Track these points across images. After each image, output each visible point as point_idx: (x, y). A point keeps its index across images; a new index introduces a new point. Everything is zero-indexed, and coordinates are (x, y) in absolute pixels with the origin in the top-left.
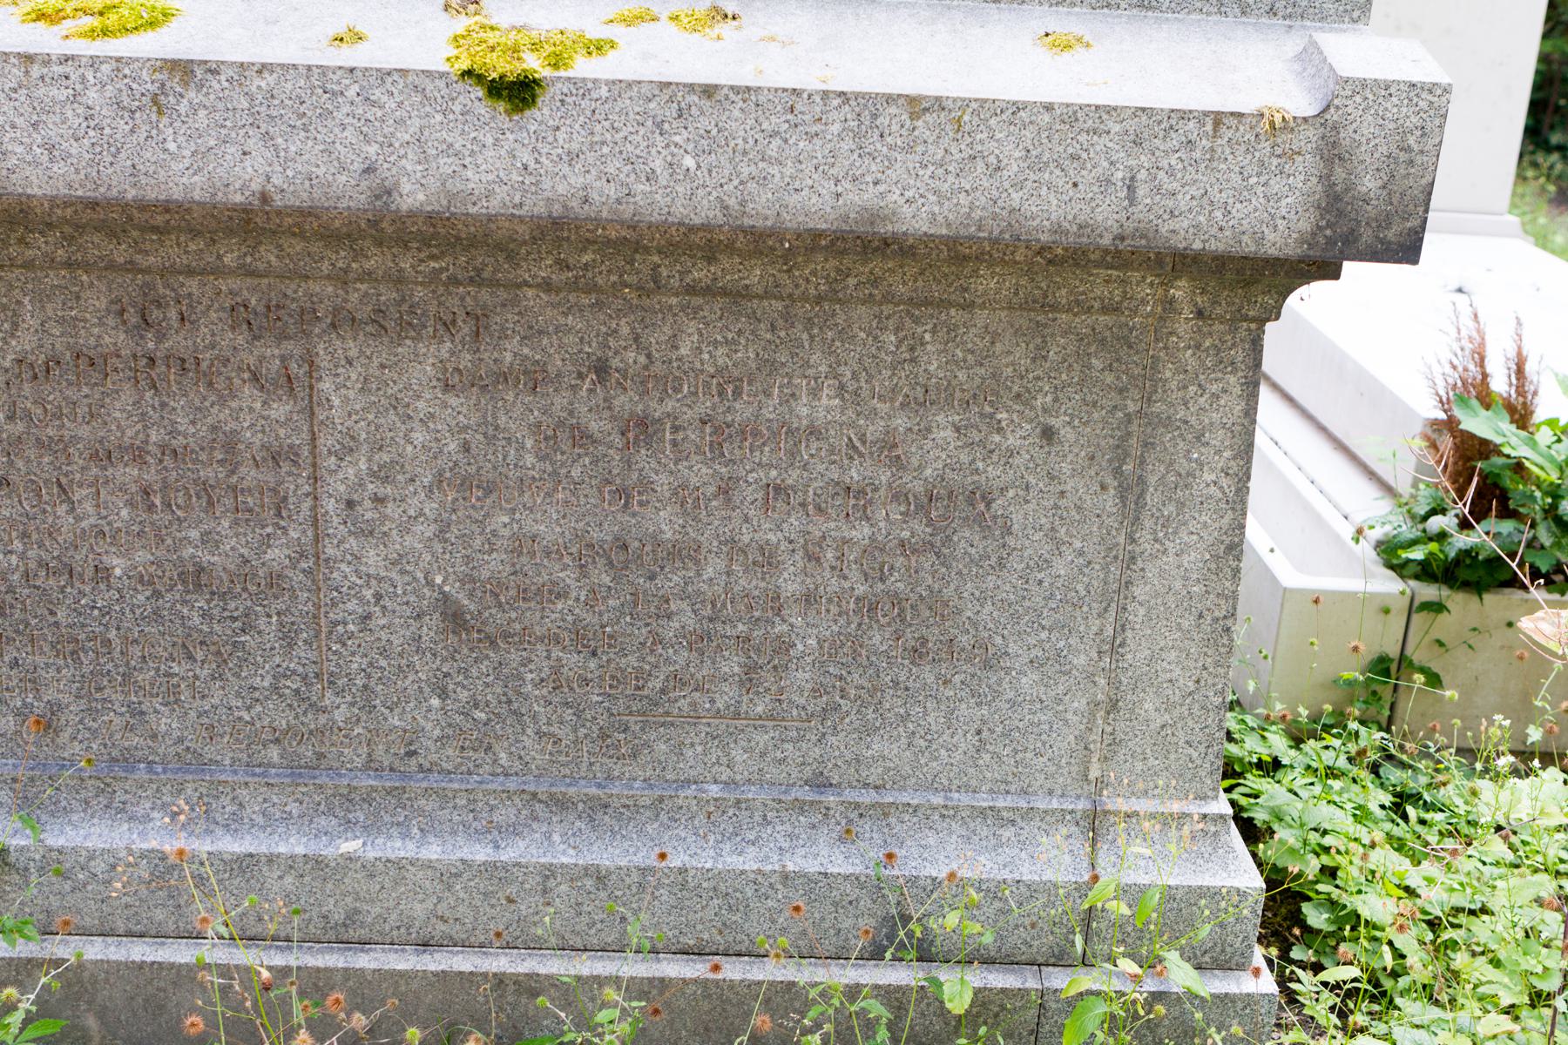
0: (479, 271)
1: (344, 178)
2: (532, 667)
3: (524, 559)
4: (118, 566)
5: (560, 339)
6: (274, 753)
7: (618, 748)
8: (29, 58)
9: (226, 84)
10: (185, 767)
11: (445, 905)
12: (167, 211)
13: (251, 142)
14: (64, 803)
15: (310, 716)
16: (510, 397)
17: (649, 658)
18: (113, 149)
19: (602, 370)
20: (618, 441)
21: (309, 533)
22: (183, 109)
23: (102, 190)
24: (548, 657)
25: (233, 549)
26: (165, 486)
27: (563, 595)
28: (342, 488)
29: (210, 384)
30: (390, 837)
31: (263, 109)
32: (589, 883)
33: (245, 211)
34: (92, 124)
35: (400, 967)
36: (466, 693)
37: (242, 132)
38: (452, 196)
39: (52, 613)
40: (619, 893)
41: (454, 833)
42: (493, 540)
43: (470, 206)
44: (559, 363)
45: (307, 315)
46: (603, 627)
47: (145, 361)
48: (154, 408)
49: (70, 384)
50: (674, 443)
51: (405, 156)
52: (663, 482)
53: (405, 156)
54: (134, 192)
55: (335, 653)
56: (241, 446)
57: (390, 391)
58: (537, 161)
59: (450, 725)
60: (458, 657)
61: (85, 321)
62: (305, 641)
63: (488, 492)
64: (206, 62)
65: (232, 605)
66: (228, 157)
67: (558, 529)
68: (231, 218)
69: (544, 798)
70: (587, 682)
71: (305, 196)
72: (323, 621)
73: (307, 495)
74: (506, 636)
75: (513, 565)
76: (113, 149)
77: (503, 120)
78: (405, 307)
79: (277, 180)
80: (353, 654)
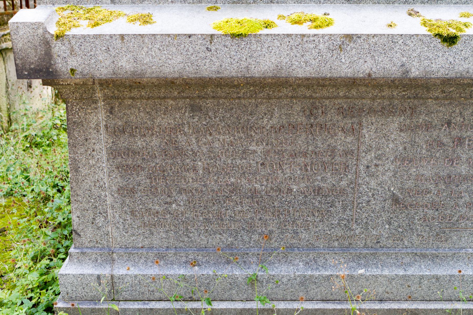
0: (417, 95)
1: (395, 68)
2: (418, 215)
3: (419, 182)
4: (295, 188)
5: (437, 114)
6: (336, 244)
7: (441, 238)
8: (304, 36)
9: (362, 41)
10: (309, 249)
11: (388, 288)
12: (330, 80)
13: (368, 58)
14: (273, 261)
15: (348, 232)
16: (420, 133)
17: (454, 211)
18: (325, 62)
19: (449, 123)
20: (451, 144)
21: (354, 176)
22: (348, 49)
23: (320, 74)
24: (423, 212)
25: (330, 182)
26: (312, 163)
27: (429, 192)
28: (366, 162)
29: (329, 132)
30: (372, 268)
31: (373, 48)
32: (434, 280)
33: (354, 79)
34: (320, 55)
35: (376, 308)
36: (397, 223)
37: (365, 55)
38: (427, 72)
39: (273, 203)
40: (443, 283)
41: (391, 266)
42: (410, 176)
43: (432, 75)
44: (436, 122)
45: (361, 110)
46: (441, 202)
47: (310, 126)
48: (311, 140)
49: (286, 133)
50: (469, 145)
51: (414, 61)
52: (464, 157)
53: (414, 61)
54: (330, 75)
55: (358, 212)
56: (336, 151)
57: (384, 132)
58: (454, 61)
59: (391, 233)
60: (395, 212)
61: (293, 114)
62: (349, 209)
63: (410, 162)
64: (357, 35)
65: (328, 199)
66: (360, 63)
67: (430, 172)
68: (349, 81)
69: (419, 254)
70: (434, 218)
71: (382, 74)
72: (355, 202)
73: (355, 165)
74: (411, 205)
75: (416, 184)
76: (325, 62)
77: (446, 49)
78: (391, 106)
79: (374, 70)
80: (364, 213)
